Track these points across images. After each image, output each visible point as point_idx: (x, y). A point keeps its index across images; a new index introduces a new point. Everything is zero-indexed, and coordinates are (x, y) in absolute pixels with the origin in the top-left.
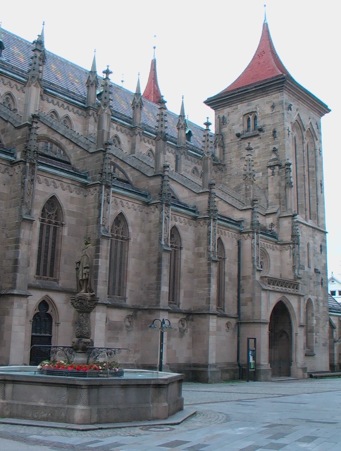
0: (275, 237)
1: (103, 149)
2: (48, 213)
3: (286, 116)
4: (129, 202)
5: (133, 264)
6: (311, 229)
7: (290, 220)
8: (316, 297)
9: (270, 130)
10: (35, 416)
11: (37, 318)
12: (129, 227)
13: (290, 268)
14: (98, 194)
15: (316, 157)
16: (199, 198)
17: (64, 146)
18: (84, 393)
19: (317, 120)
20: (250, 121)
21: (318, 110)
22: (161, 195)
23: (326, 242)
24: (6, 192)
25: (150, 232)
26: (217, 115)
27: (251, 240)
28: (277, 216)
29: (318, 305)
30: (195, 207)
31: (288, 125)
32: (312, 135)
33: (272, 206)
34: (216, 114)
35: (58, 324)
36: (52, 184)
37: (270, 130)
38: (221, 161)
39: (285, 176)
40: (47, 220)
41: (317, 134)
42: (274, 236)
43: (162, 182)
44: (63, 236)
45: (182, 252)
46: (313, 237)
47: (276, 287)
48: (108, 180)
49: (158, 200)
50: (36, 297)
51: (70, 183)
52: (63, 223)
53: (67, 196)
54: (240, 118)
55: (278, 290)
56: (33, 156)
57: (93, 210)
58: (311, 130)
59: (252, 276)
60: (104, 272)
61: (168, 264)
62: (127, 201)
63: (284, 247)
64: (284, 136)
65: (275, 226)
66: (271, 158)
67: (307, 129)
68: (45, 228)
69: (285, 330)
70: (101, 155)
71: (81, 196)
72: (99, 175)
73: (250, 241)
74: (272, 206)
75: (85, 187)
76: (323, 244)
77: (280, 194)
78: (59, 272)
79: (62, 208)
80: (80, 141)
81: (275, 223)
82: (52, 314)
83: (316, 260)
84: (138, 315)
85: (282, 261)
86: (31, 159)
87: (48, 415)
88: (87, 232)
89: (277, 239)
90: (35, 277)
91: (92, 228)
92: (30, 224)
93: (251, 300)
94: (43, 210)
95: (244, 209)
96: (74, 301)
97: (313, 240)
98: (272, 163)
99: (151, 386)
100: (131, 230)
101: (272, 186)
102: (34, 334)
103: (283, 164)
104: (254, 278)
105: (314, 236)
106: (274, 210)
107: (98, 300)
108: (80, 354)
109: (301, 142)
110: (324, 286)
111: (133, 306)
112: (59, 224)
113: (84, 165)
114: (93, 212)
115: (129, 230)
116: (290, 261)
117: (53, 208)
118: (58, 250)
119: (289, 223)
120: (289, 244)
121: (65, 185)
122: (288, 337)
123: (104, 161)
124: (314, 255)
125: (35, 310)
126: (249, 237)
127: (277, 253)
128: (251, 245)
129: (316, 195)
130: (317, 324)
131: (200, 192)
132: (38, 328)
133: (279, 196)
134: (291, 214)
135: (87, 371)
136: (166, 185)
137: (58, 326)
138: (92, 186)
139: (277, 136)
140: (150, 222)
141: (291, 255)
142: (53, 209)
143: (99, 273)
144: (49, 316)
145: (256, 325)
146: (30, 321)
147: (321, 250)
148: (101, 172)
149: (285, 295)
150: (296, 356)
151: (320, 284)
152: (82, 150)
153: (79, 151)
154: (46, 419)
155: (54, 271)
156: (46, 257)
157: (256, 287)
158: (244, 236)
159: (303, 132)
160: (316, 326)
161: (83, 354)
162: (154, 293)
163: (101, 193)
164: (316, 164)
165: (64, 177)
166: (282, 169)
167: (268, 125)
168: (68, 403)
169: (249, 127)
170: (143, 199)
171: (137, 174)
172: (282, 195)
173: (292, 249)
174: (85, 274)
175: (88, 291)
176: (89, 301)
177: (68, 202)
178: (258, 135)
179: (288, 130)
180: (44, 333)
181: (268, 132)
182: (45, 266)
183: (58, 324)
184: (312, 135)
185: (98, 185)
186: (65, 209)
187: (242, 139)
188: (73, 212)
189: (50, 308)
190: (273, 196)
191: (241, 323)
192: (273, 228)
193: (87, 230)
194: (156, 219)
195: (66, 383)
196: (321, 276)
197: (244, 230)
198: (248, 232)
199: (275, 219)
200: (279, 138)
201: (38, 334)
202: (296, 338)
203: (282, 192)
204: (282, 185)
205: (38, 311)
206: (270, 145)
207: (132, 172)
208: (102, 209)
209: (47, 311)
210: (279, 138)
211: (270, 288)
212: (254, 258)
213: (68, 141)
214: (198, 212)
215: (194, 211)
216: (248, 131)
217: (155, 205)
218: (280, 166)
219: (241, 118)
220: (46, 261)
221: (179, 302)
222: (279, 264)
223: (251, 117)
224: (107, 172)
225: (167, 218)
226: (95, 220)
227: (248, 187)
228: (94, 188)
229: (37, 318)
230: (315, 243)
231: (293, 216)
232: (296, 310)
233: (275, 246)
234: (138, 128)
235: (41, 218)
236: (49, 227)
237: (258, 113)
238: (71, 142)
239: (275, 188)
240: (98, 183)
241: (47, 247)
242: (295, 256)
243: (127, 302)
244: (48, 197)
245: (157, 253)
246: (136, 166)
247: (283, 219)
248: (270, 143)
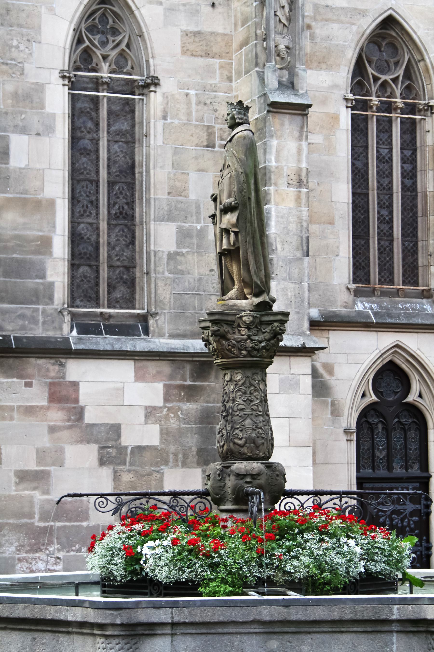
2: (376, 79)
11: (374, 420)
24: (220, 30)
79: (426, 57)
90: (348, 289)
92: (299, 118)
94: (359, 68)
99: (395, 627)
102: (368, 472)
146: (346, 431)
155: (420, 264)
176: (249, 328)
182: (386, 252)
209: (406, 396)
229: (374, 420)
235: (351, 96)
236: (385, 127)
244: (368, 24)
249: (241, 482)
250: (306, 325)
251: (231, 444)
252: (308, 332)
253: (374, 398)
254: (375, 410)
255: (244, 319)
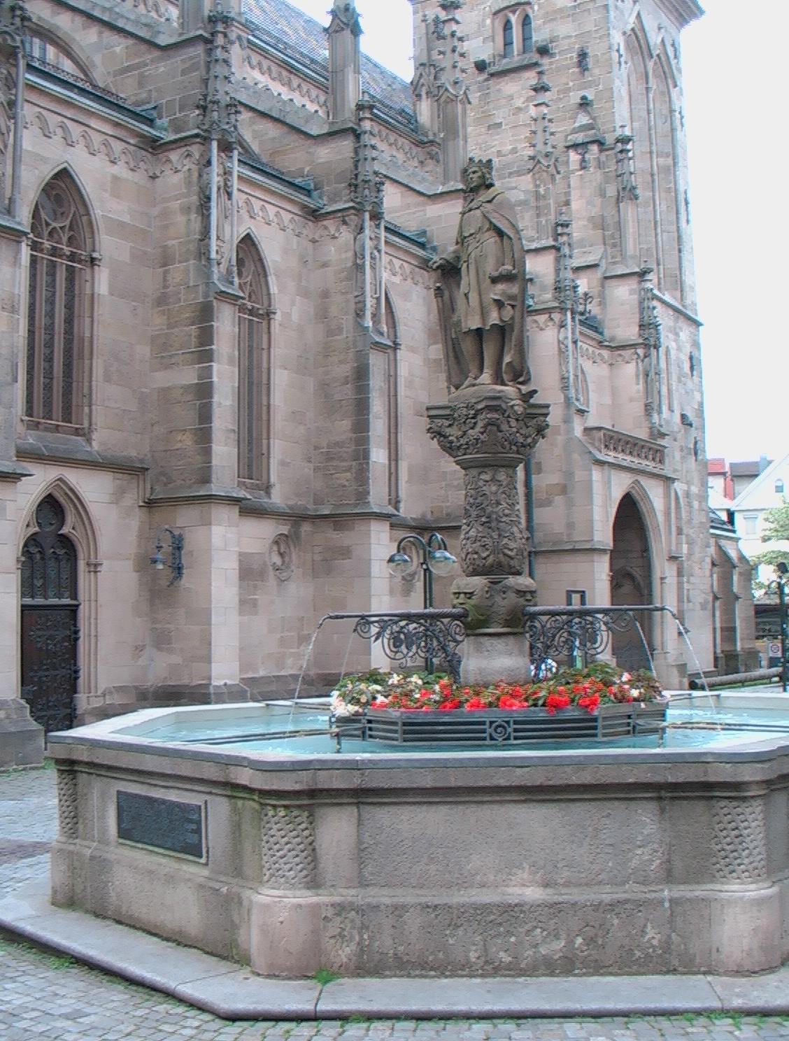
0: (596, 329)
1: (206, 35)
2: (48, 224)
3: (612, 14)
4: (267, 206)
5: (285, 388)
6: (671, 312)
7: (633, 283)
8: (685, 487)
9: (570, 50)
10: (502, 954)
11: (34, 550)
12: (269, 278)
13: (638, 408)
14: (195, 168)
15: (673, 130)
16: (435, 210)
17: (66, 33)
18: (752, 820)
19: (674, 34)
20: (511, 28)
21: (677, 10)
22: (356, 186)
23: (699, 349)
25: (325, 294)
26: (421, 14)
27: (556, 330)
28: (599, 274)
29: (690, 505)
30: (424, 233)
31: (617, 39)
32: (664, 73)
33: (584, 250)
34: (415, 12)
35: (94, 567)
36: (59, 131)
37: (570, 50)
38: (434, 134)
39: (616, 170)
40: (47, 245)
41: (675, 72)
42: (592, 325)
43: (356, 151)
44: (96, 296)
45: (398, 358)
46: (677, 334)
47: (621, 456)
48: (226, 127)
49: (346, 202)
50: (39, 481)
51: (111, 133)
52: (95, 255)
53: (104, 173)
54: (484, 20)
55: (625, 464)
56: (12, 24)
57: (181, 219)
58: (663, 59)
59: (563, 426)
60: (228, 403)
61: (382, 384)
62: (262, 203)
63: (620, 355)
64: (611, 67)
65: (596, 301)
66: (577, 125)
67: (655, 53)
68: (43, 268)
69: (629, 569)
70: (199, 50)
71: (140, 177)
72: (197, 112)
73: (556, 334)
74: (584, 250)
75: (150, 150)
76: (695, 354)
77: (603, 217)
78: (90, 406)
79: (92, 212)
80: (122, 16)
81: (595, 292)
82: (78, 536)
83: (683, 392)
84: (303, 534)
85: (614, 392)
86: (6, 32)
87: (571, 942)
88: (165, 287)
89: (601, 334)
91: (183, 272)
93: (564, 490)
95: (533, 247)
96: (447, 423)
97: (676, 341)
98: (580, 138)
100: (274, 289)
101: (581, 197)
102: (28, 601)
103: (610, 139)
104: (570, 431)
105: (678, 330)
106: (591, 260)
107: (546, 415)
108: (499, 644)
109: (642, 87)
110: (700, 458)
111: (290, 507)
112: (83, 258)
113: (141, 84)
114: (184, 225)
115: (271, 287)
116: (638, 392)
117: (61, 210)
118: (82, 339)
119: (632, 292)
120: (634, 346)
121: (97, 139)
122: (637, 588)
123: (208, 69)
124: (680, 381)
125: (28, 526)
126: (550, 324)
127: (603, 370)
128: (556, 344)
129: (675, 227)
130: (690, 554)
131: (438, 192)
132: (38, 583)
133: (600, 224)
134: (637, 270)
135: (596, 713)
136: (369, 159)
137: (96, 572)
138: (174, 146)
139: (590, 66)
140: (325, 265)
141: (641, 376)
142: (62, 214)
143: (215, 406)
144: (67, 544)
145: (568, 557)
147: (692, 368)
148: (202, 103)
149: (640, 478)
150: (662, 637)
151: (693, 452)
152: (130, 42)
153: (120, 45)
154: (566, 966)
156: (49, 359)
157: (576, 456)
158: (536, 321)
159: (647, 60)
160: (688, 559)
161: (511, 640)
162: (349, 469)
163: (209, 163)
164: (674, 147)
165: (93, 113)
166: (607, 153)
167: (563, 38)
168: (669, 876)
169: (508, 43)
170: (303, 198)
171: (272, 131)
172: (610, 221)
173: (643, 361)
174: (499, 304)
175: (505, 377)
176: (517, 420)
177: (105, 191)
178: (536, 64)
179: (618, 51)
180: (55, 596)
181: (564, 57)
183: (96, 565)
184: (664, 73)
185: (198, 140)
186: (98, 212)
187: (492, 75)
188: (122, 225)
189: (70, 518)
190: (586, 223)
191: (536, 553)
192: (589, 307)
193: (165, 279)
194: (344, 256)
195: (658, 779)
196: (694, 432)
197: (536, 304)
198: (548, 311)
199: (595, 283)
200: (595, 71)
201: (39, 601)
202: (662, 589)
203: (610, 212)
204: (608, 194)
205: (37, 529)
206: (569, 90)
207: (256, 128)
208: (214, 211)
210: (596, 71)
211: (610, 460)
212: (568, 378)
213: (79, 20)
214: (434, 249)
215: (422, 246)
216: (505, 56)
217: (340, 215)
218: (600, 143)
219: (488, 21)
220: (49, 374)
221: (397, 497)
222: (607, 400)
223: (514, 19)
224: (223, 104)
225: (375, 252)
226: (193, 247)
227: (542, 191)
228: (184, 149)
229: (34, 550)
230: (679, 349)
231: (642, 275)
232: (660, 517)
233: (597, 351)
234: (236, 24)
236: (53, 266)
237: (536, 7)
238: (90, 21)
239: (588, 203)
240: (197, 136)
241: (50, 329)
242: (649, 377)
243: (272, 496)
244: (48, 171)
245: (351, 355)
246: (271, 110)
247: (613, 282)
248: (571, 84)
249: (521, 599)
250: (13, 452)
251: (501, 555)
252: (15, 459)
253: (37, 529)
254: (35, 540)
255: (516, 408)
